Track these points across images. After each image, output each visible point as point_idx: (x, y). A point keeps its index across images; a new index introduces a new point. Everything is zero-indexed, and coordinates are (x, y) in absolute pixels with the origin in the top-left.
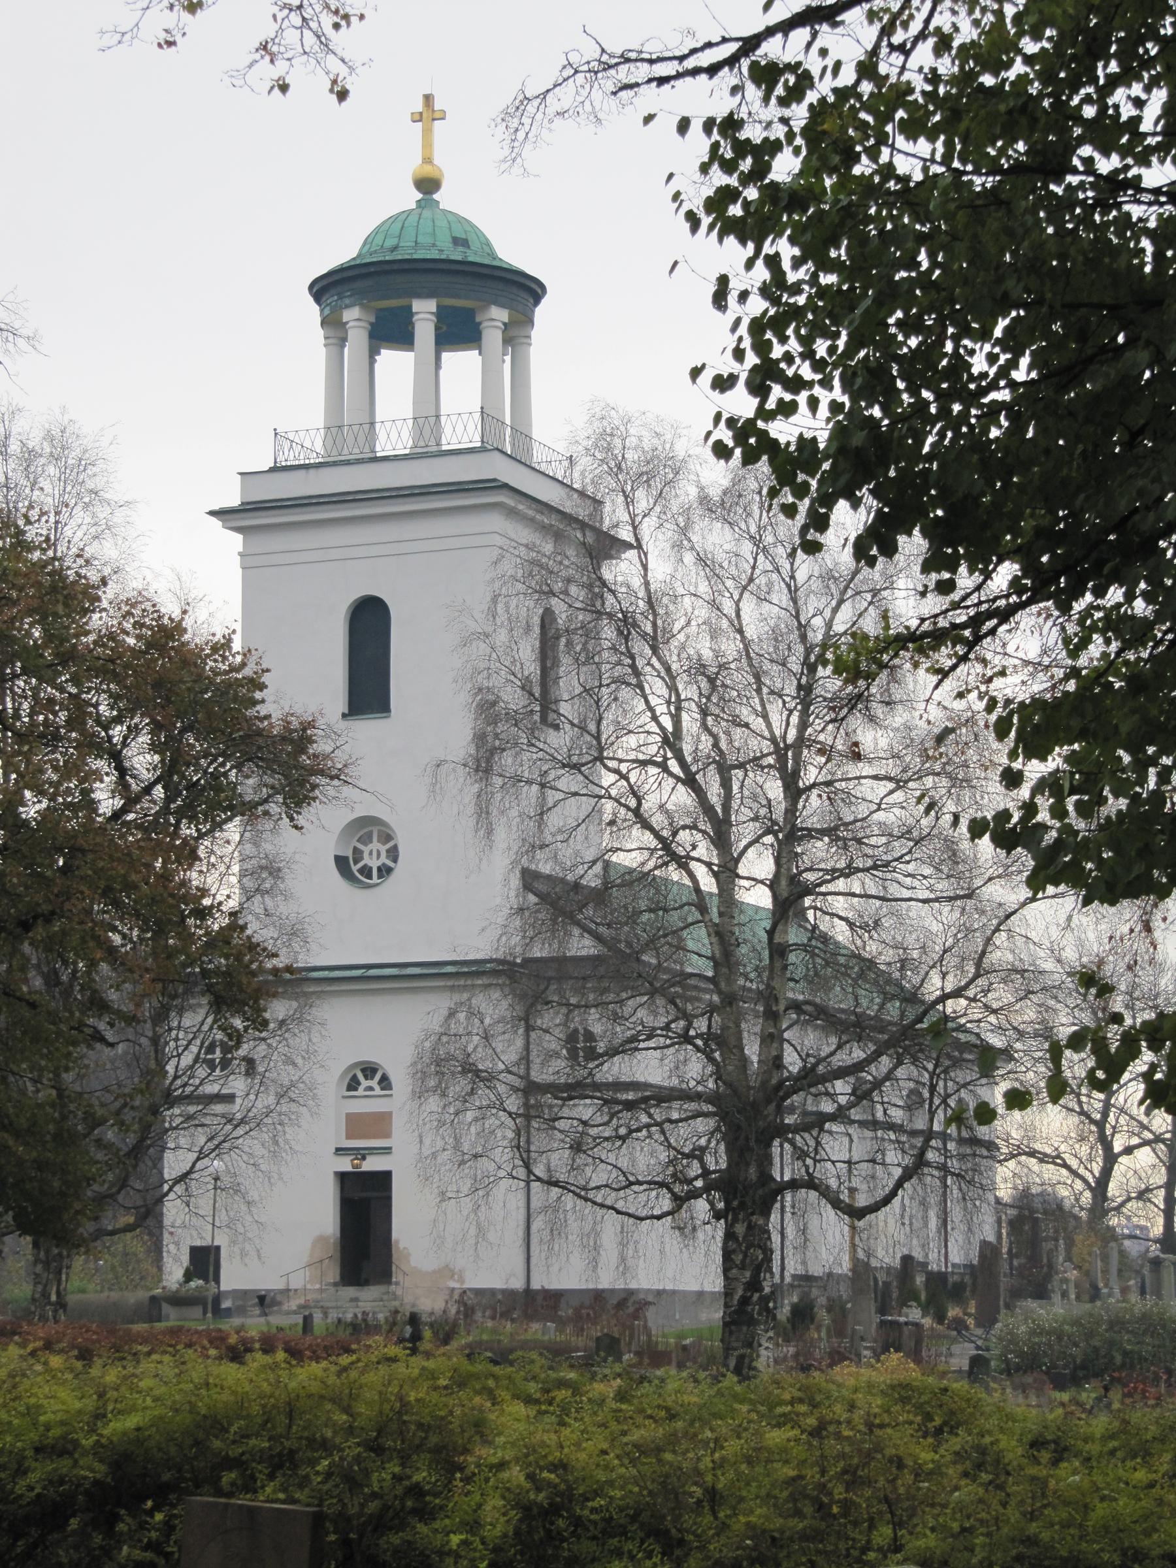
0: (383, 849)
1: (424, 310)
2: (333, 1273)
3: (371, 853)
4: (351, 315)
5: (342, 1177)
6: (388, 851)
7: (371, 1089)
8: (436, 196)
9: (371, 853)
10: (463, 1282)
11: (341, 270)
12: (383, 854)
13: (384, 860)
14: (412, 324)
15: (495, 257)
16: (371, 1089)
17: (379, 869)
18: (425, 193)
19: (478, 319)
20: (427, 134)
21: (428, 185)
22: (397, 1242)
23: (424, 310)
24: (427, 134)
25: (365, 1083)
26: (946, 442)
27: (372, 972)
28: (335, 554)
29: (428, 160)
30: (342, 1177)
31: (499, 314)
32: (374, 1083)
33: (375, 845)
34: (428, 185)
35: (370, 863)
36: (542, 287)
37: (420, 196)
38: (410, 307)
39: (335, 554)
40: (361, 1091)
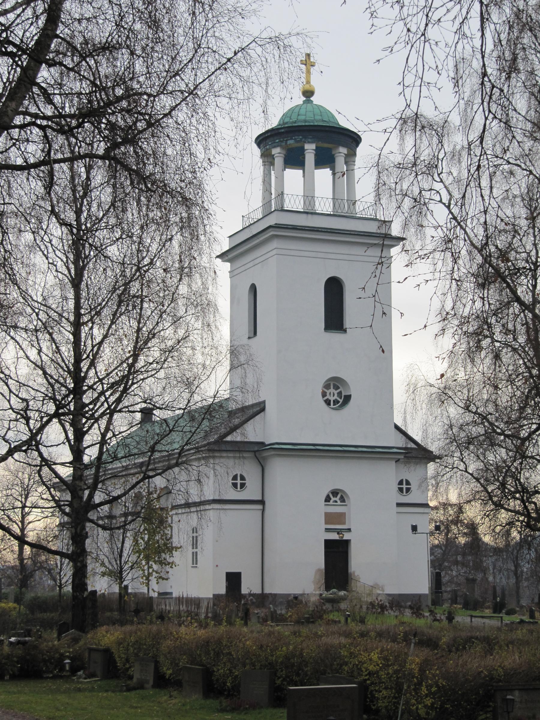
0: (336, 392)
1: (310, 148)
2: (323, 587)
3: (330, 394)
4: (276, 151)
5: (328, 543)
6: (338, 393)
7: (336, 502)
8: (312, 99)
9: (330, 394)
10: (383, 591)
11: (272, 130)
12: (336, 395)
13: (336, 397)
14: (304, 155)
15: (338, 124)
16: (336, 502)
17: (334, 401)
18: (306, 97)
19: (333, 153)
20: (308, 72)
21: (308, 94)
22: (354, 572)
23: (310, 148)
25: (333, 499)
27: (299, 447)
28: (320, 255)
29: (308, 82)
30: (328, 543)
31: (343, 150)
32: (337, 499)
33: (332, 390)
34: (308, 94)
35: (330, 398)
37: (305, 99)
38: (303, 147)
39: (320, 255)
40: (331, 502)
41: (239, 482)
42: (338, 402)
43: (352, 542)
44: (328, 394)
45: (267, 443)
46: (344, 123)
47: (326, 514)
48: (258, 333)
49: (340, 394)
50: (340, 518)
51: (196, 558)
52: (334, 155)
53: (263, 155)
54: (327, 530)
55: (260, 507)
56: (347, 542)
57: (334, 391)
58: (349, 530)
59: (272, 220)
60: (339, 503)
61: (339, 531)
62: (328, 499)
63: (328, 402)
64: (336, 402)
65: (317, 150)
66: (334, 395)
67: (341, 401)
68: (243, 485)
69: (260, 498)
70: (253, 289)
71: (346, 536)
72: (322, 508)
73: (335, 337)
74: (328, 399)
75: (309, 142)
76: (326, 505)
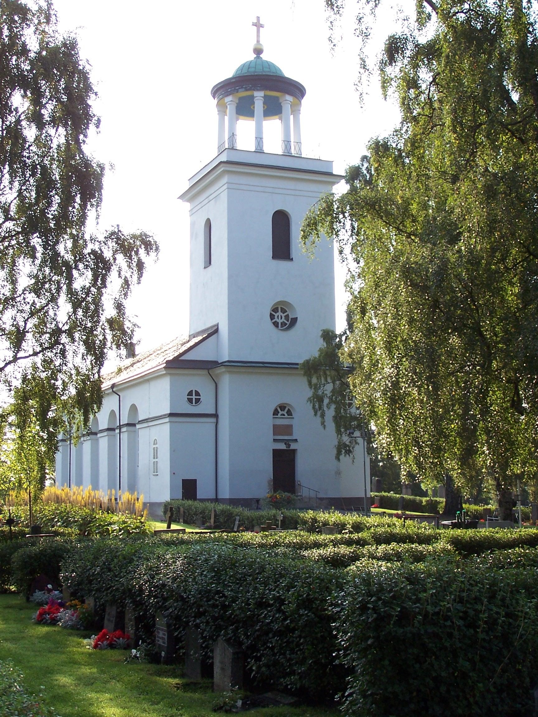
5: (276, 452)
8: (261, 56)
12: (283, 318)
13: (283, 320)
16: (284, 415)
20: (258, 32)
21: (258, 51)
24: (258, 32)
25: (281, 412)
26: (4, 135)
29: (258, 41)
30: (276, 452)
31: (289, 98)
32: (285, 413)
33: (280, 313)
34: (258, 51)
36: (390, 38)
37: (255, 56)
40: (279, 416)
41: (194, 397)
42: (286, 324)
43: (298, 451)
44: (276, 317)
45: (220, 362)
46: (288, 73)
47: (274, 426)
48: (212, 263)
49: (287, 317)
50: (288, 429)
51: (157, 453)
52: (280, 103)
53: (218, 105)
54: (275, 440)
55: (213, 420)
56: (294, 451)
57: (282, 314)
58: (296, 440)
59: (224, 158)
60: (286, 416)
61: (287, 443)
62: (276, 413)
63: (276, 324)
64: (283, 324)
65: (265, 97)
66: (281, 318)
67: (288, 323)
68: (198, 401)
69: (215, 413)
70: (208, 225)
71: (293, 446)
72: (269, 421)
73: (283, 264)
74: (276, 321)
75: (258, 90)
76: (274, 418)
